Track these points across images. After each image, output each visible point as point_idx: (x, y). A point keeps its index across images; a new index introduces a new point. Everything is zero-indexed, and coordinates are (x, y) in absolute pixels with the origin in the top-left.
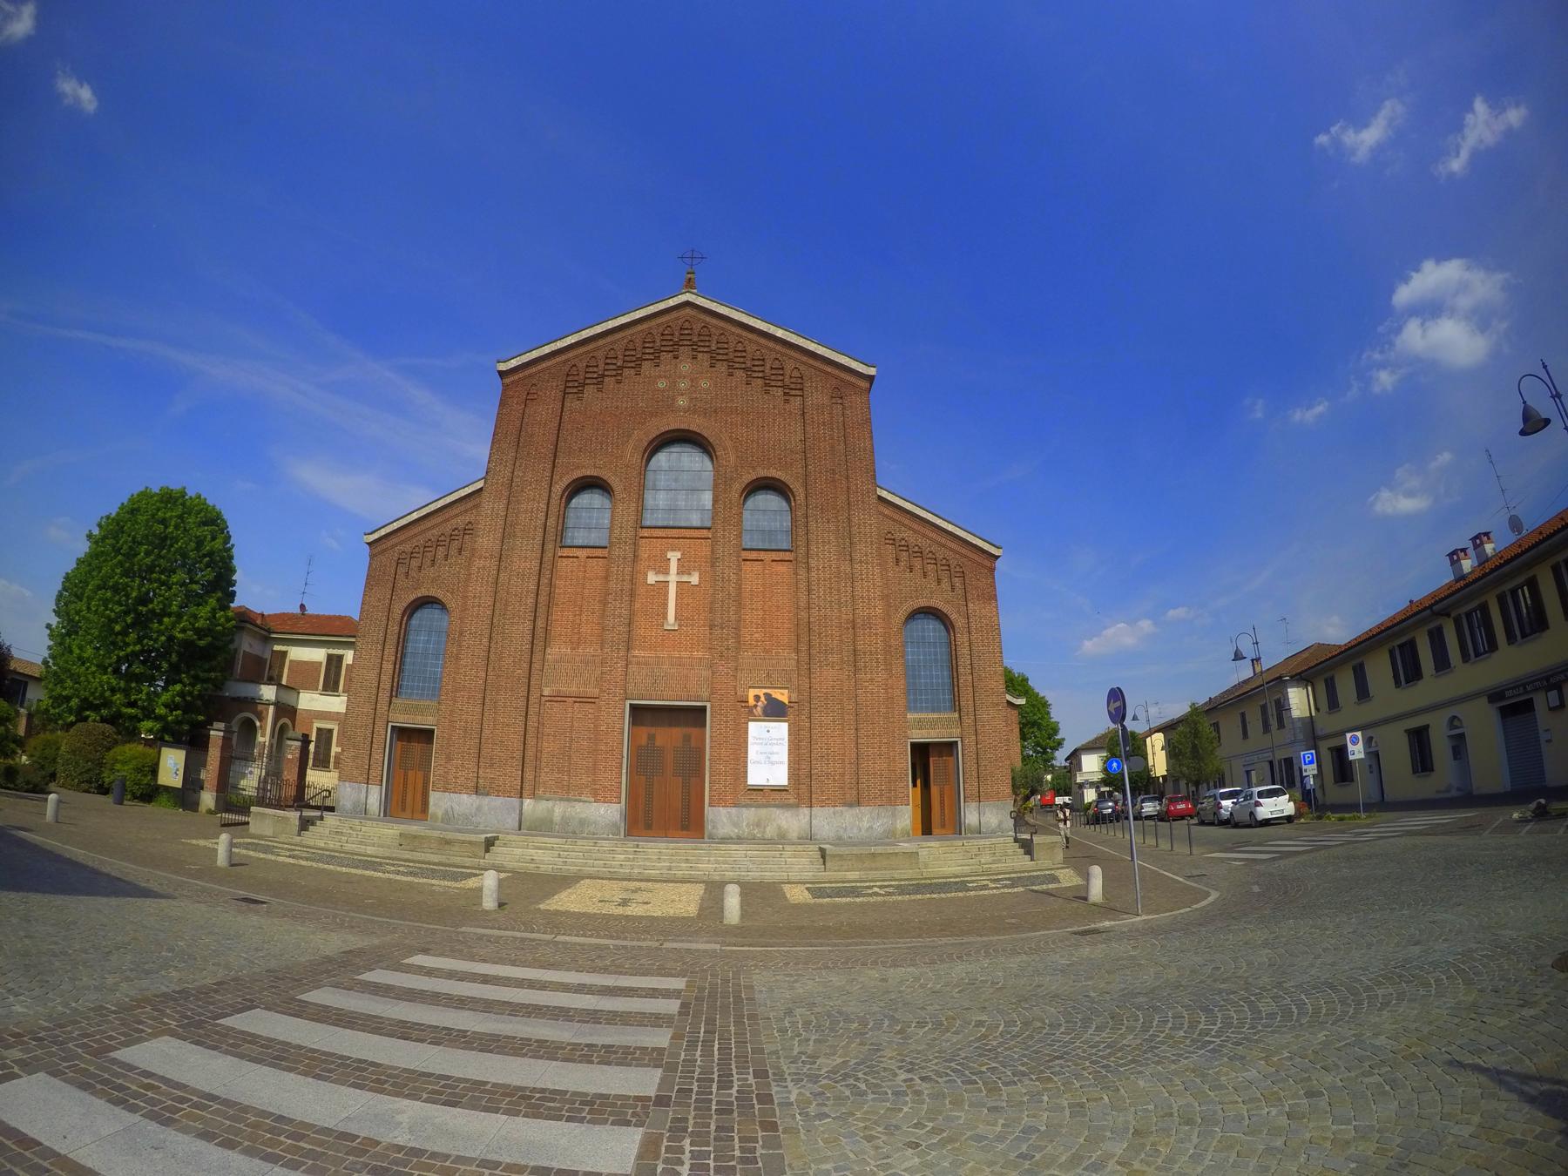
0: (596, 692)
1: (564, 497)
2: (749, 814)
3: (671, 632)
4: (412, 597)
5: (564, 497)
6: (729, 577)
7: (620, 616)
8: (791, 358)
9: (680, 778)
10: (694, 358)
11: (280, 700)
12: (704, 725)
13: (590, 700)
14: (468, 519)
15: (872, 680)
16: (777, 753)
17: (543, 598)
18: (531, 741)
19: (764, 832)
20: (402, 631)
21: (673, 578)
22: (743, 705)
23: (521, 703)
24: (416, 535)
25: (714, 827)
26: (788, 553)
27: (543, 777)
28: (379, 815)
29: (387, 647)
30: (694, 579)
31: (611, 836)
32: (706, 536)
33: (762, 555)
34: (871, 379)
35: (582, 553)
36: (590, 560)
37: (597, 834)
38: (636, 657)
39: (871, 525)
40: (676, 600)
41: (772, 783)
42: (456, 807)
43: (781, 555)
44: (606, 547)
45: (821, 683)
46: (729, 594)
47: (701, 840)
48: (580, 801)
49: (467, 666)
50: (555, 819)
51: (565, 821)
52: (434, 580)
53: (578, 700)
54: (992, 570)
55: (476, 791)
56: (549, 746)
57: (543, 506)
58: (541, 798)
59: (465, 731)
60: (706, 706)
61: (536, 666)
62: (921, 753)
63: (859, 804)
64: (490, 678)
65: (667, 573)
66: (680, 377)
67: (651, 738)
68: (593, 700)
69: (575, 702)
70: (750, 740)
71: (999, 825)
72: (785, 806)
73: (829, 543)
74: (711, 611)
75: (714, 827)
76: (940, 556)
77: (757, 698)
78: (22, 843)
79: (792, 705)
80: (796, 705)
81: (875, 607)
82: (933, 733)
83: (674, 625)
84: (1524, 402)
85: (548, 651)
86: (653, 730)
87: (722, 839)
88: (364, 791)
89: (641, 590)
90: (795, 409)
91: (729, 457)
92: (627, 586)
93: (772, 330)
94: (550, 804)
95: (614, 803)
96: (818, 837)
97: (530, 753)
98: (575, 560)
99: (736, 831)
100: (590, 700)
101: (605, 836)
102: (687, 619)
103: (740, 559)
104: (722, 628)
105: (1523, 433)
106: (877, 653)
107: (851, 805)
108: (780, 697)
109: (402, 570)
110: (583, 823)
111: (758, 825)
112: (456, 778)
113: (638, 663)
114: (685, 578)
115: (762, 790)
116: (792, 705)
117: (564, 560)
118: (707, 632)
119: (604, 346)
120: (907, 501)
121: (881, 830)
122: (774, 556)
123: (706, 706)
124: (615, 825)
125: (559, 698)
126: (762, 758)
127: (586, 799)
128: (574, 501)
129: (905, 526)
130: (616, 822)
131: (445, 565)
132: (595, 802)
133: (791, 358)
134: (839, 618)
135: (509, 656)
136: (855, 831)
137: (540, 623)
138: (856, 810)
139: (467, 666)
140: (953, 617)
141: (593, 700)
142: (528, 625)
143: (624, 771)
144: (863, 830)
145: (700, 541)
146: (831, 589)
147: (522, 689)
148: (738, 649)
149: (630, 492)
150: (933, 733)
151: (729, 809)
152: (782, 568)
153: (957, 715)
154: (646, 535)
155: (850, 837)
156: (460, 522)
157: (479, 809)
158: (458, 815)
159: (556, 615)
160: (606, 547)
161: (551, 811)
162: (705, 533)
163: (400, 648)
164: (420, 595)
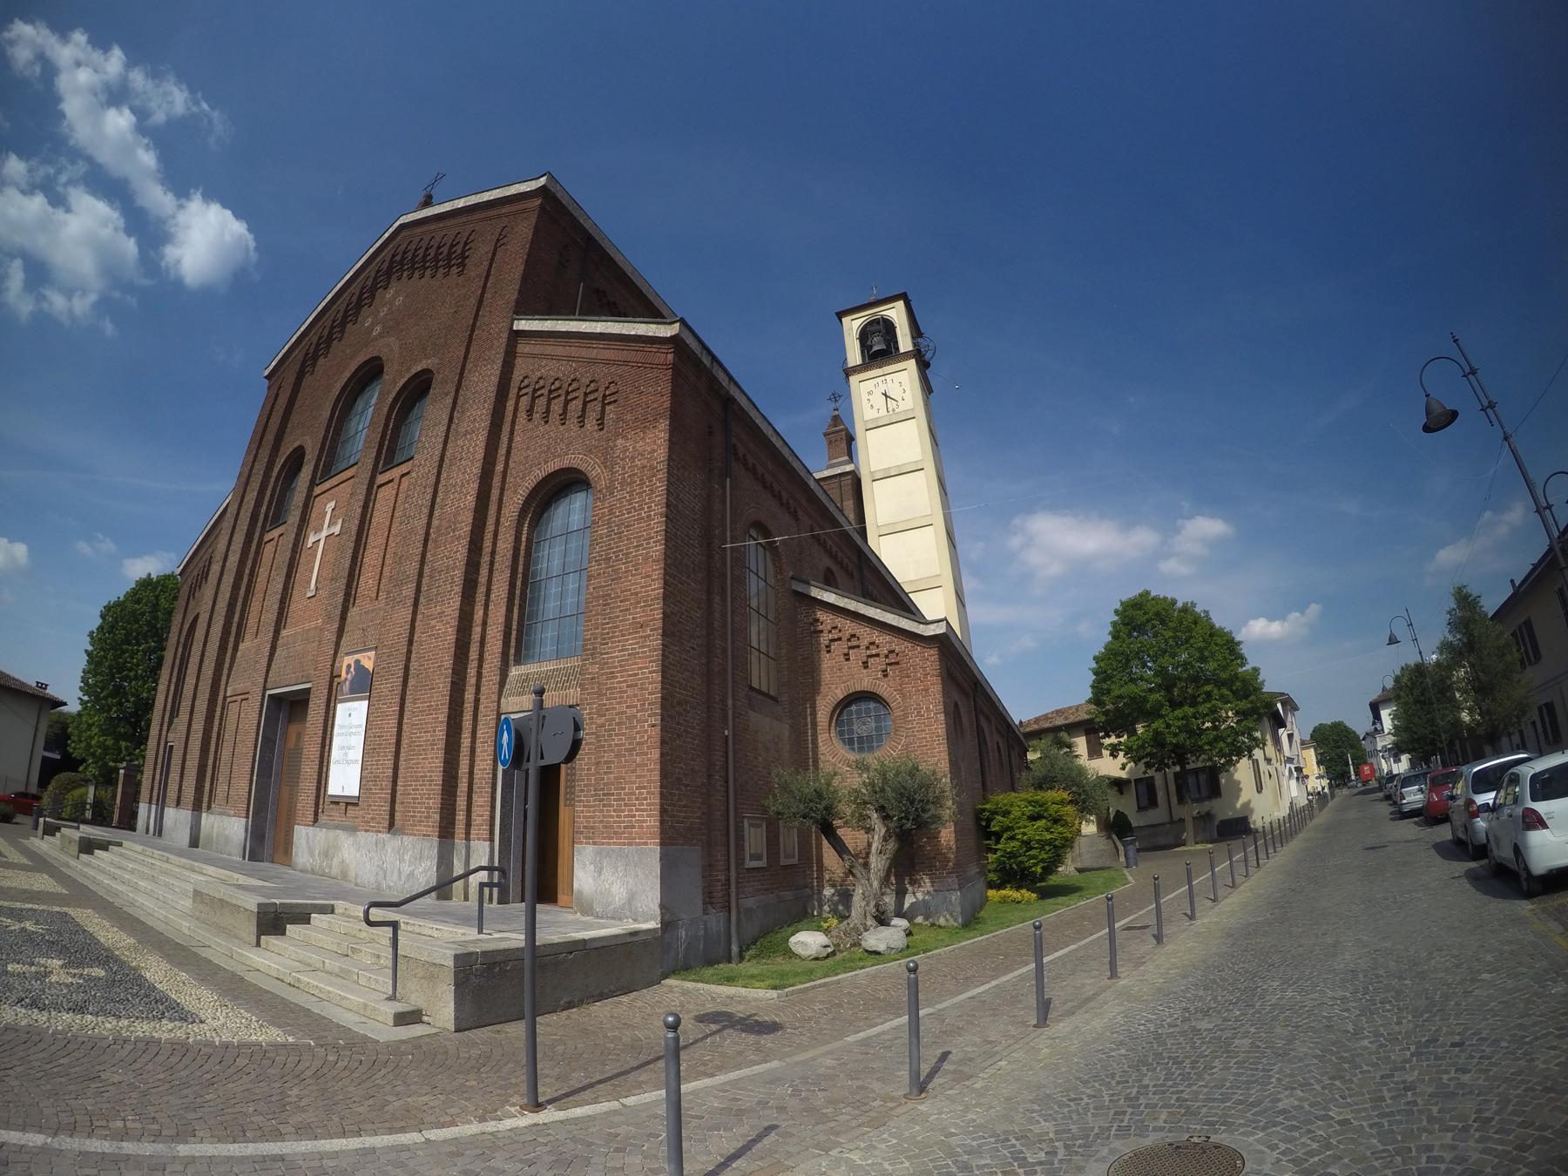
155: (390, 888)
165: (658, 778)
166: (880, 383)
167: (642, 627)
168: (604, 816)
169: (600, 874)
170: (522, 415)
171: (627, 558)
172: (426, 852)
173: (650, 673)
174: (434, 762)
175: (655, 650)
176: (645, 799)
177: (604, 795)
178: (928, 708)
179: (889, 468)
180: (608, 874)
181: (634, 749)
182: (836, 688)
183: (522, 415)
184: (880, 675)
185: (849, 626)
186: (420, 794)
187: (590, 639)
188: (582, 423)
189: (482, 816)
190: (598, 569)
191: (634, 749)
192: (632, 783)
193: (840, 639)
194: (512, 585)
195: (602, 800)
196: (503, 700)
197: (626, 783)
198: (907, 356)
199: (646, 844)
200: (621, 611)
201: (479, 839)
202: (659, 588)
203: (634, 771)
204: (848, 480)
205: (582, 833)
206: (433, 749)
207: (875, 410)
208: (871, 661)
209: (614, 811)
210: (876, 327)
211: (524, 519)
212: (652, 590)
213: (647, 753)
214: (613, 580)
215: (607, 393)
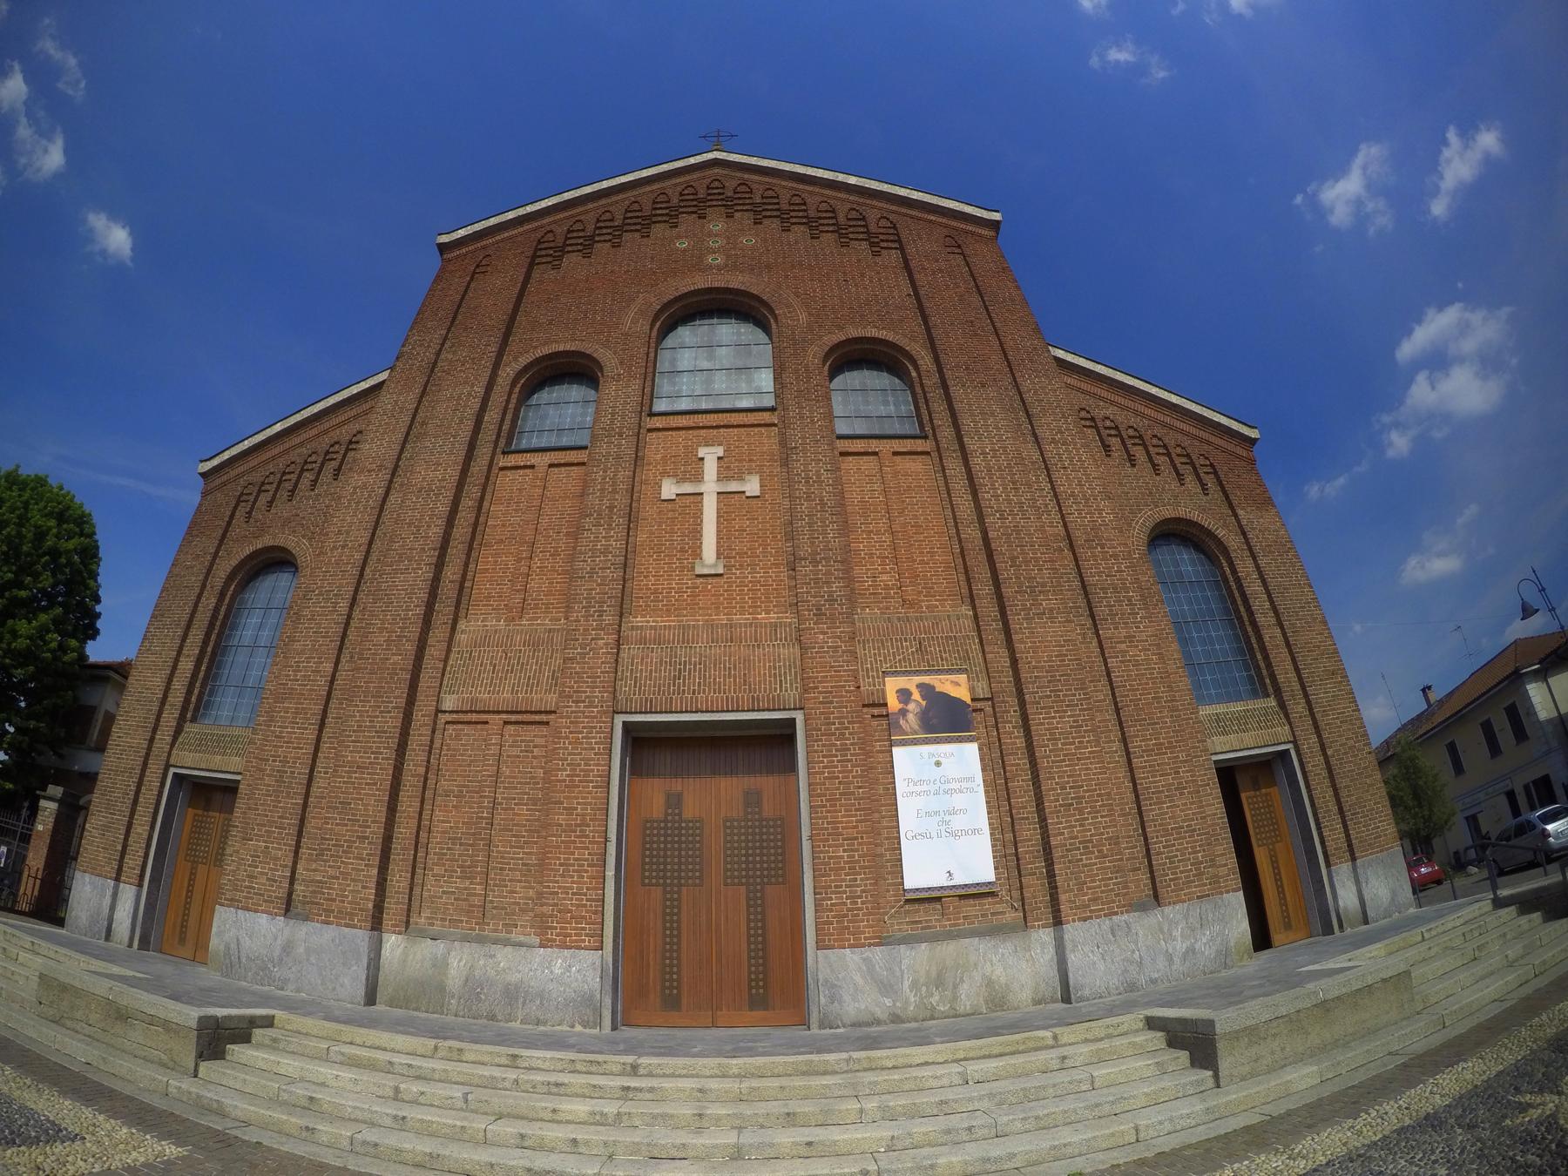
0: (551, 700)
1: (517, 390)
2: (916, 960)
3: (710, 580)
4: (248, 550)
5: (517, 390)
6: (818, 475)
7: (605, 552)
8: (874, 207)
9: (743, 889)
10: (730, 216)
12: (792, 767)
13: (537, 718)
16: (964, 811)
17: (461, 532)
18: (408, 804)
19: (955, 998)
20: (223, 609)
21: (710, 486)
22: (876, 711)
23: (393, 722)
25: (832, 999)
27: (431, 887)
28: (130, 945)
29: (193, 631)
32: (769, 422)
33: (874, 445)
34: (995, 225)
35: (541, 460)
36: (556, 470)
37: (545, 1024)
38: (638, 628)
40: (718, 522)
41: (959, 880)
42: (246, 943)
43: (908, 445)
44: (585, 448)
46: (823, 504)
47: (799, 1032)
48: (506, 943)
49: (303, 652)
50: (450, 982)
51: (474, 988)
53: (513, 718)
54: (1252, 462)
55: (287, 907)
56: (445, 820)
57: (479, 390)
58: (422, 934)
59: (280, 781)
60: (794, 719)
61: (434, 651)
62: (1230, 776)
63: (1157, 899)
64: (341, 675)
65: (698, 477)
66: (710, 236)
67: (674, 801)
68: (544, 718)
69: (506, 723)
70: (901, 787)
71: (1393, 899)
72: (996, 931)
73: (992, 414)
74: (790, 536)
76: (1169, 441)
77: (904, 695)
79: (979, 705)
80: (987, 706)
81: (1100, 511)
82: (1248, 738)
83: (715, 566)
85: (462, 625)
86: (677, 785)
87: (853, 1025)
88: (109, 893)
89: (649, 511)
91: (794, 316)
92: (621, 500)
93: (841, 177)
94: (441, 946)
95: (586, 948)
96: (1087, 992)
97: (404, 831)
99: (888, 1002)
100: (537, 718)
102: (741, 554)
103: (836, 453)
104: (815, 563)
107: (1142, 907)
108: (954, 692)
110: (513, 994)
111: (939, 982)
112: (251, 877)
113: (642, 640)
114: (733, 486)
115: (939, 899)
116: (979, 705)
117: (509, 473)
118: (784, 576)
120: (1099, 363)
121: (1210, 952)
122: (897, 445)
124: (587, 1000)
125: (473, 716)
126: (932, 825)
127: (522, 938)
128: (535, 396)
129: (1101, 398)
130: (592, 996)
132: (542, 946)
133: (874, 207)
134: (1041, 529)
135: (381, 630)
136: (1161, 963)
137: (451, 573)
138: (1155, 917)
139: (303, 652)
140: (1221, 533)
141: (544, 718)
142: (426, 573)
143: (610, 873)
145: (756, 430)
147: (398, 692)
148: (852, 598)
149: (630, 368)
150: (1248, 738)
151: (867, 952)
152: (916, 466)
153: (1272, 702)
154: (659, 425)
155: (1154, 981)
156: (344, 434)
157: (288, 948)
158: (248, 957)
159: (486, 560)
160: (585, 448)
161: (441, 965)
162: (766, 417)
163: (213, 637)
164: (259, 546)
172: (1211, 915)
174: (1190, 809)
181: (1362, 773)
186: (1177, 850)
192: (1370, 800)
194: (205, 642)
196: (174, 752)
197: (1365, 801)
199: (1392, 847)
203: (1368, 791)
205: (1334, 855)
206: (1181, 794)
209: (1364, 826)
211: (233, 580)
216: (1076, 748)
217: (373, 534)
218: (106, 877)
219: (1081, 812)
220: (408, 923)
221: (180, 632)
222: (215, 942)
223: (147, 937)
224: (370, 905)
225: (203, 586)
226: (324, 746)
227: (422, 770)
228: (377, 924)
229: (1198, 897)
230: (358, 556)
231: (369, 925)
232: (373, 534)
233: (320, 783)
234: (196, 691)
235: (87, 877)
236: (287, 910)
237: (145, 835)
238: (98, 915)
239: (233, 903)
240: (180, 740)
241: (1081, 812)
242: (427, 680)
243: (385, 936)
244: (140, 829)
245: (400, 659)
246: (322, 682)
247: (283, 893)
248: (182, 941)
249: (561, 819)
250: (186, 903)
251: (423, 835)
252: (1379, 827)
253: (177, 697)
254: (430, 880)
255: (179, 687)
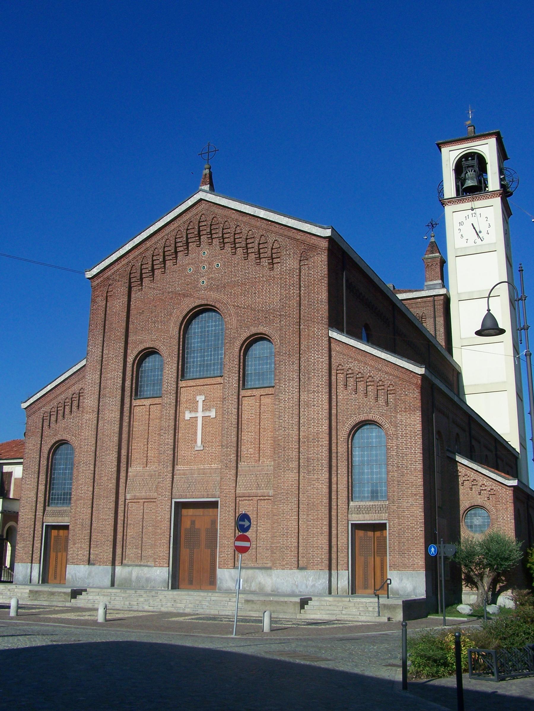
4: (53, 441)
6: (232, 410)
9: (210, 550)
11: (6, 509)
14: (81, 386)
15: (318, 479)
19: (251, 586)
20: (50, 463)
24: (51, 400)
26: (271, 389)
28: (39, 583)
29: (41, 475)
30: (213, 414)
31: (163, 589)
38: (179, 470)
39: (322, 362)
42: (78, 574)
45: (284, 482)
46: (232, 423)
49: (82, 484)
50: (133, 578)
52: (65, 429)
55: (89, 562)
56: (131, 532)
59: (82, 525)
68: (154, 500)
75: (220, 583)
78: (427, 685)
81: (322, 425)
84: (489, 310)
90: (277, 275)
95: (165, 567)
98: (144, 407)
100: (152, 500)
101: (160, 589)
104: (227, 447)
105: (478, 333)
106: (322, 460)
109: (46, 424)
110: (148, 580)
112: (77, 555)
119: (151, 246)
123: (46, 525)
131: (70, 419)
136: (304, 587)
139: (82, 484)
141: (154, 500)
142: (115, 455)
144: (309, 587)
146: (292, 414)
147: (112, 497)
155: (301, 592)
156: (76, 389)
157: (90, 574)
158: (78, 578)
159: (135, 445)
161: (131, 573)
165: (424, 548)
166: (470, 216)
167: (415, 495)
168: (403, 561)
169: (402, 581)
170: (341, 387)
171: (407, 468)
173: (419, 512)
175: (421, 504)
176: (419, 555)
177: (402, 553)
178: (507, 516)
179: (473, 292)
180: (405, 581)
181: (414, 538)
182: (466, 503)
183: (341, 387)
184: (486, 499)
185: (473, 475)
187: (391, 496)
188: (377, 399)
189: (344, 561)
190: (392, 469)
191: (414, 538)
193: (468, 480)
195: (402, 555)
197: (411, 549)
198: (493, 194)
199: (420, 570)
200: (406, 488)
201: (342, 570)
202: (421, 482)
204: (440, 302)
207: (464, 239)
208: (482, 492)
210: (470, 162)
212: (419, 482)
213: (419, 540)
214: (401, 475)
215: (389, 389)
216: (290, 517)
217: (96, 439)
218: (27, 563)
219: (287, 537)
220: (122, 563)
221: (36, 475)
222: (68, 576)
223: (45, 579)
224: (111, 559)
225: (40, 457)
226: (94, 513)
227: (123, 518)
228: (113, 564)
229: (320, 570)
230: (93, 449)
231: (111, 564)
232: (96, 439)
233: (94, 525)
234: (47, 495)
235: (20, 564)
236: (89, 563)
237: (39, 547)
238: (26, 575)
239: (73, 563)
240: (45, 513)
241: (287, 537)
242: (121, 490)
243: (116, 567)
244: (37, 545)
245: (112, 485)
246: (90, 493)
247: (87, 558)
248: (55, 578)
249: (159, 531)
250: (55, 566)
251: (125, 537)
252: (415, 561)
253: (41, 499)
254: (127, 550)
255: (41, 495)
